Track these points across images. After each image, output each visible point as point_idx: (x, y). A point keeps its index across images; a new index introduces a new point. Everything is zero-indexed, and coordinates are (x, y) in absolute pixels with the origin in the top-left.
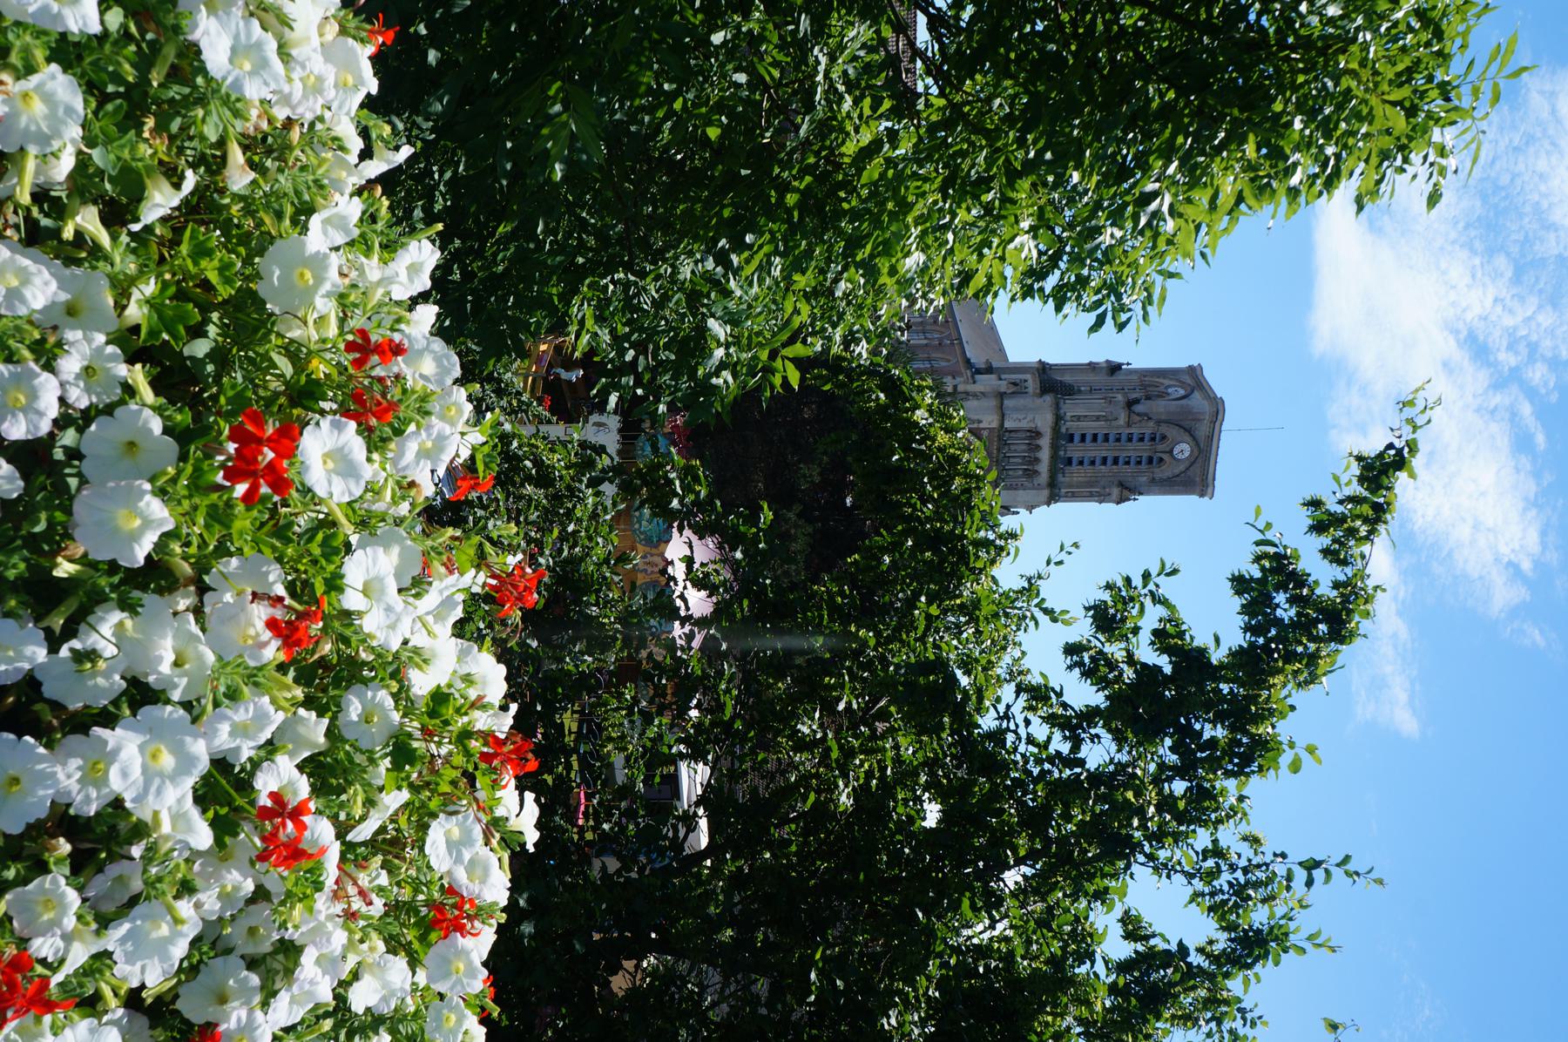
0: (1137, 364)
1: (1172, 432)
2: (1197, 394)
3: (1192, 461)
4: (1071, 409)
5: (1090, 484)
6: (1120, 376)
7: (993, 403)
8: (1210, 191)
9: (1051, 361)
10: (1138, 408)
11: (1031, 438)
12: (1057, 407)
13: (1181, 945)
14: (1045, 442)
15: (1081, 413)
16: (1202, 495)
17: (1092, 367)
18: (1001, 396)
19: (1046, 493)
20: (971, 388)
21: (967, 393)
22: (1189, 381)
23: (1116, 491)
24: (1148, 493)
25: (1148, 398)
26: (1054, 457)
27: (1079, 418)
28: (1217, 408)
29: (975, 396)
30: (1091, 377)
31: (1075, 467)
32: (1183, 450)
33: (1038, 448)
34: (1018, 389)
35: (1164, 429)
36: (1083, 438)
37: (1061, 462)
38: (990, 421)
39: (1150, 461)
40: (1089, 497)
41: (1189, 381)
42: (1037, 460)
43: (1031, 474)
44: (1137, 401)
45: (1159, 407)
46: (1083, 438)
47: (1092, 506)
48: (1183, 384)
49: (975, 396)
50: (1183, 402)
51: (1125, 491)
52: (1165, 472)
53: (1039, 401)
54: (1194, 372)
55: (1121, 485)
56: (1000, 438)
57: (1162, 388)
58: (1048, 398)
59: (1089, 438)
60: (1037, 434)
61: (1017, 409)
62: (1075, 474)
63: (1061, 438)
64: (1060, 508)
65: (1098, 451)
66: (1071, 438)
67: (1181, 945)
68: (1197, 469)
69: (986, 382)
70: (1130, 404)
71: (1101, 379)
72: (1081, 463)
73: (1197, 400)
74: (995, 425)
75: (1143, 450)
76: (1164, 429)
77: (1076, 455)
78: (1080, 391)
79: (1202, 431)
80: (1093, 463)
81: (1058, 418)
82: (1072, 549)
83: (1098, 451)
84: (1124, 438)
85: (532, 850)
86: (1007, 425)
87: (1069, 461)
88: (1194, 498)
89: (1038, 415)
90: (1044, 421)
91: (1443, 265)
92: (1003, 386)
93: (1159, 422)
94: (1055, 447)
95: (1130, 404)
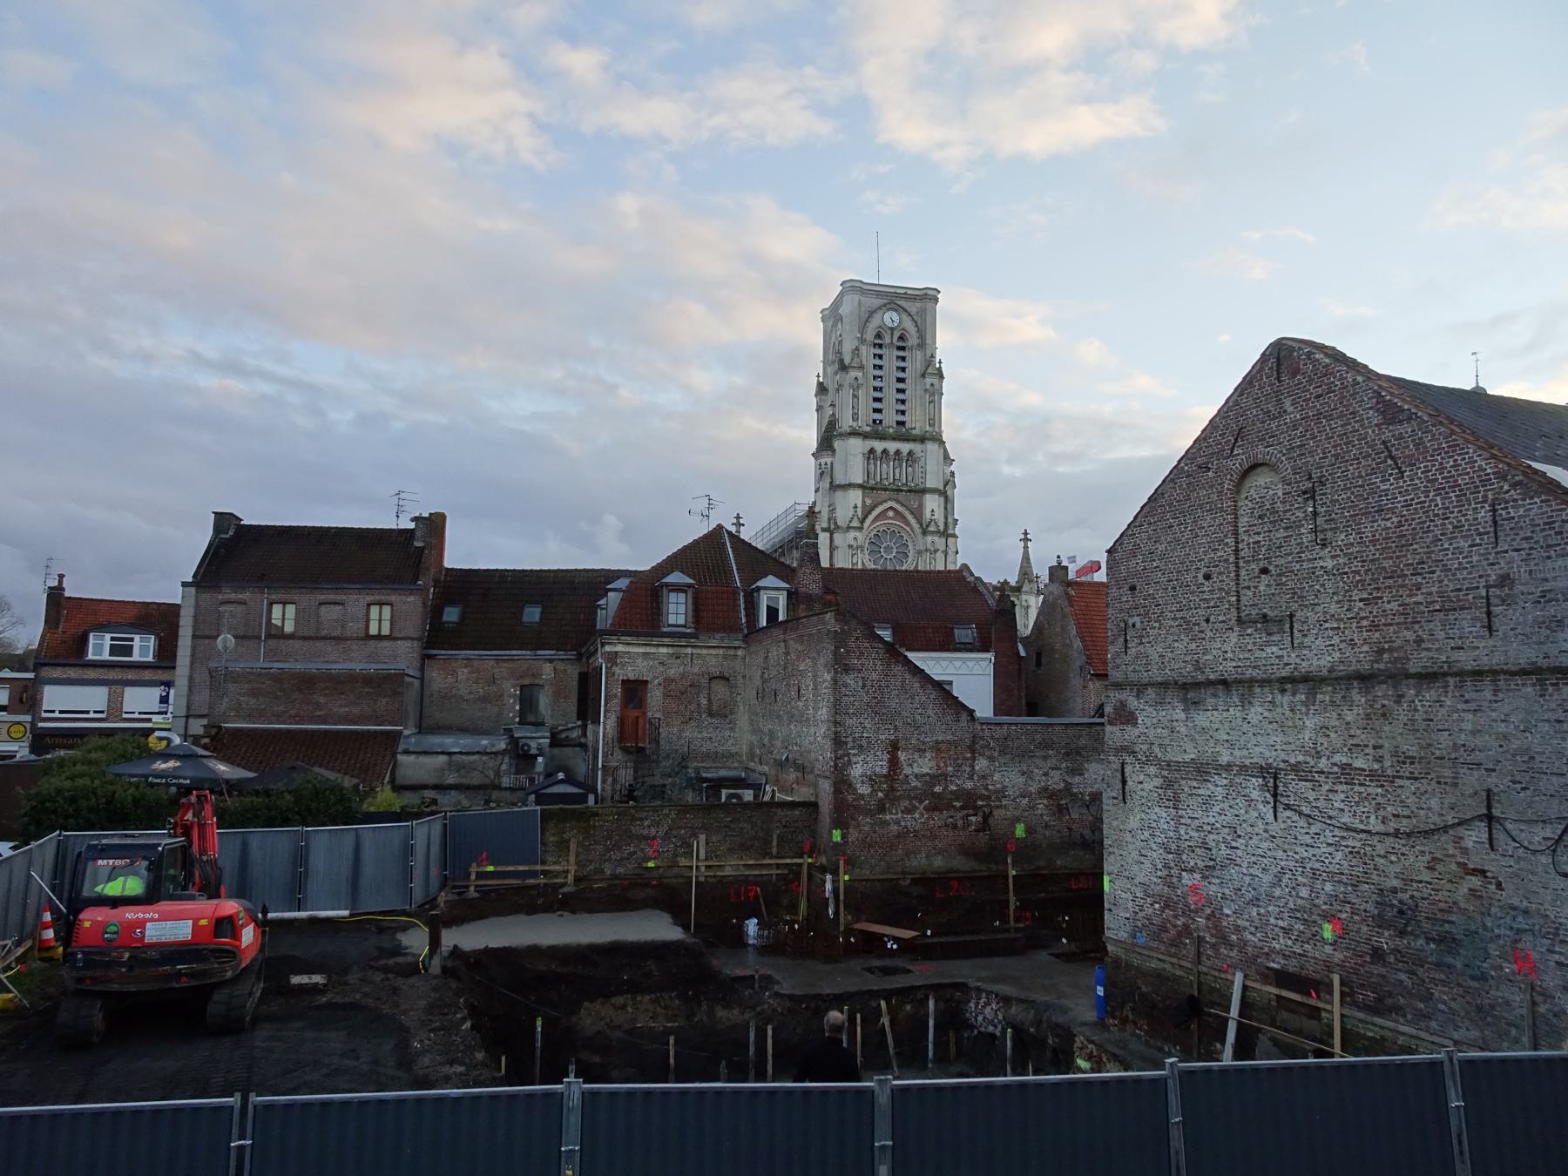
4: (846, 423)
7: (839, 494)
10: (847, 360)
14: (879, 446)
35: (870, 336)
58: (837, 444)
65: (890, 395)
74: (859, 493)
75: (890, 355)
81: (854, 433)
83: (890, 395)
90: (857, 446)
93: (862, 341)
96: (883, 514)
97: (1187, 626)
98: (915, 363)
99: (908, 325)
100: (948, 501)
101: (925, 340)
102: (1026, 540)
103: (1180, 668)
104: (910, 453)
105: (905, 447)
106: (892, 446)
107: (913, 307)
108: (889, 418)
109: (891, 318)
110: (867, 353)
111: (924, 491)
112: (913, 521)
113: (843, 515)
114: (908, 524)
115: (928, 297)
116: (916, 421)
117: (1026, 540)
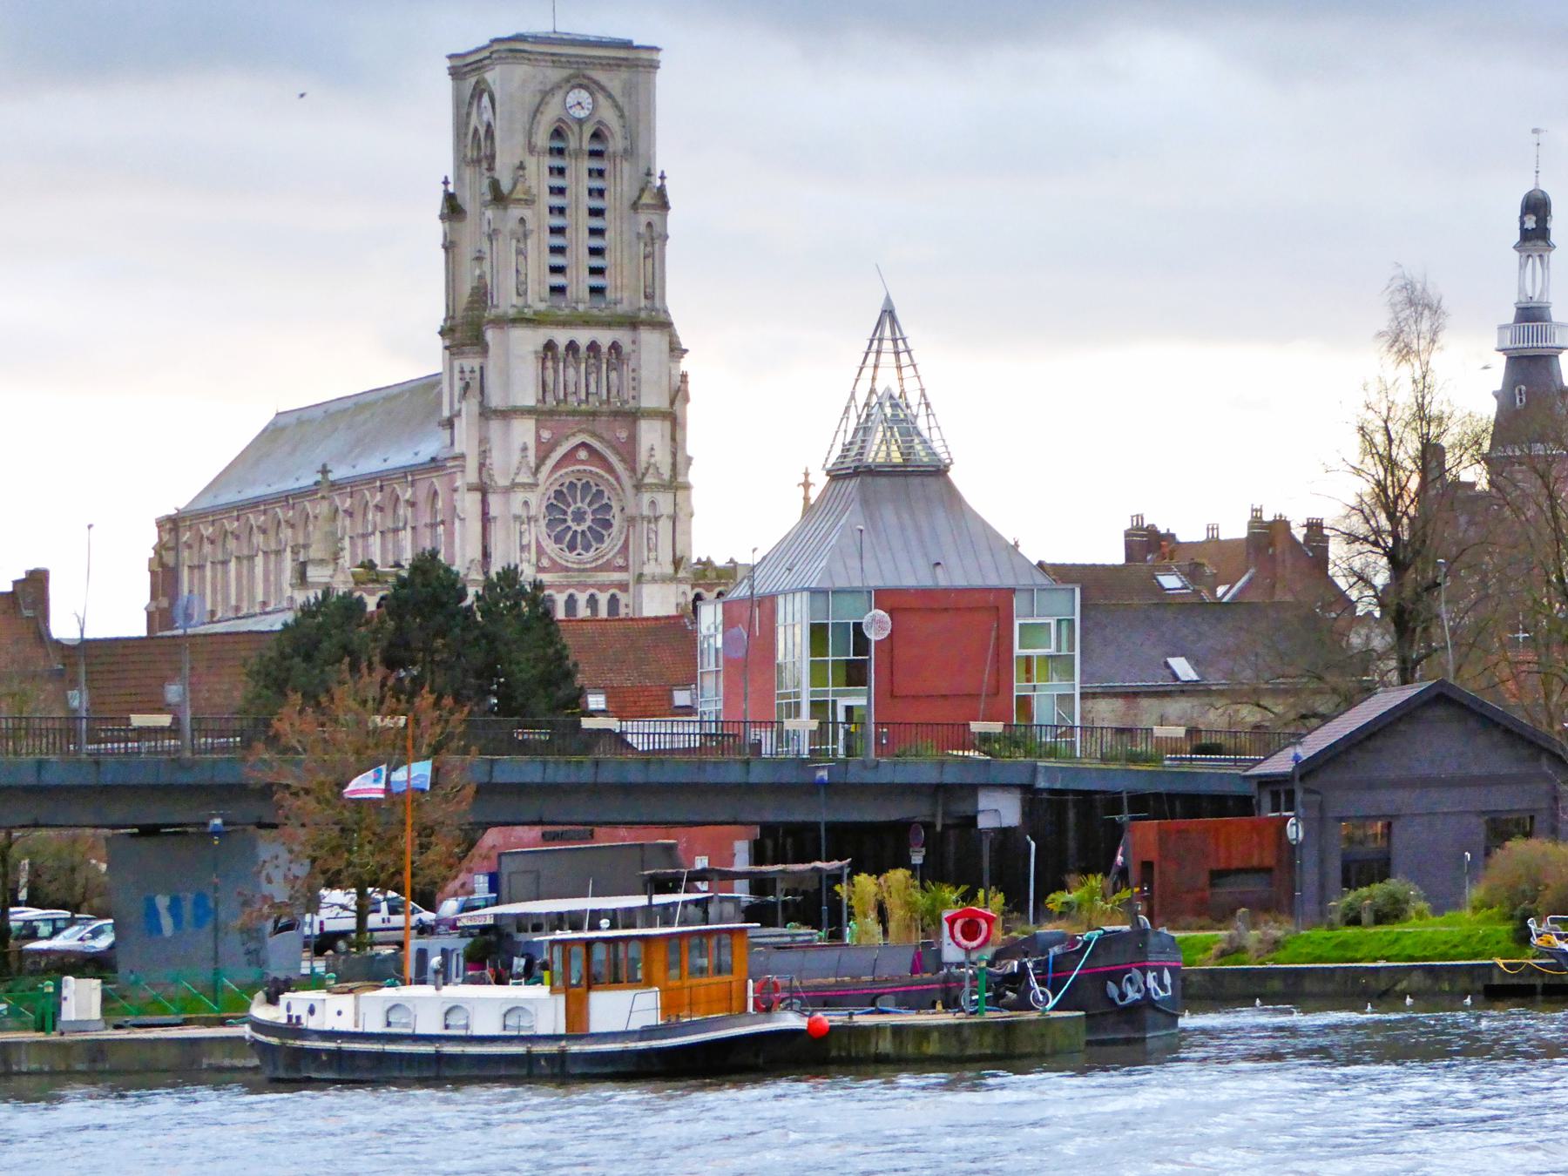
4: (506, 300)
6: (467, 201)
7: (495, 426)
8: (41, 924)
9: (441, 314)
10: (506, 186)
11: (555, 359)
13: (1315, 527)
14: (562, 337)
15: (520, 277)
16: (653, 66)
18: (486, 413)
20: (472, 464)
21: (482, 466)
24: (650, 158)
29: (484, 454)
38: (524, 431)
44: (495, 185)
49: (484, 454)
58: (490, 335)
59: (558, 261)
61: (506, 385)
66: (558, 290)
67: (1315, 527)
78: (481, 277)
80: (596, 252)
84: (557, 201)
85: (1474, 475)
86: (530, 401)
87: (596, 291)
90: (527, 341)
92: (470, 407)
95: (499, 198)
96: (569, 457)
98: (621, 187)
99: (608, 115)
101: (637, 148)
104: (615, 347)
105: (605, 337)
106: (583, 337)
107: (613, 81)
109: (579, 102)
114: (610, 469)
115: (634, 61)
116: (623, 293)
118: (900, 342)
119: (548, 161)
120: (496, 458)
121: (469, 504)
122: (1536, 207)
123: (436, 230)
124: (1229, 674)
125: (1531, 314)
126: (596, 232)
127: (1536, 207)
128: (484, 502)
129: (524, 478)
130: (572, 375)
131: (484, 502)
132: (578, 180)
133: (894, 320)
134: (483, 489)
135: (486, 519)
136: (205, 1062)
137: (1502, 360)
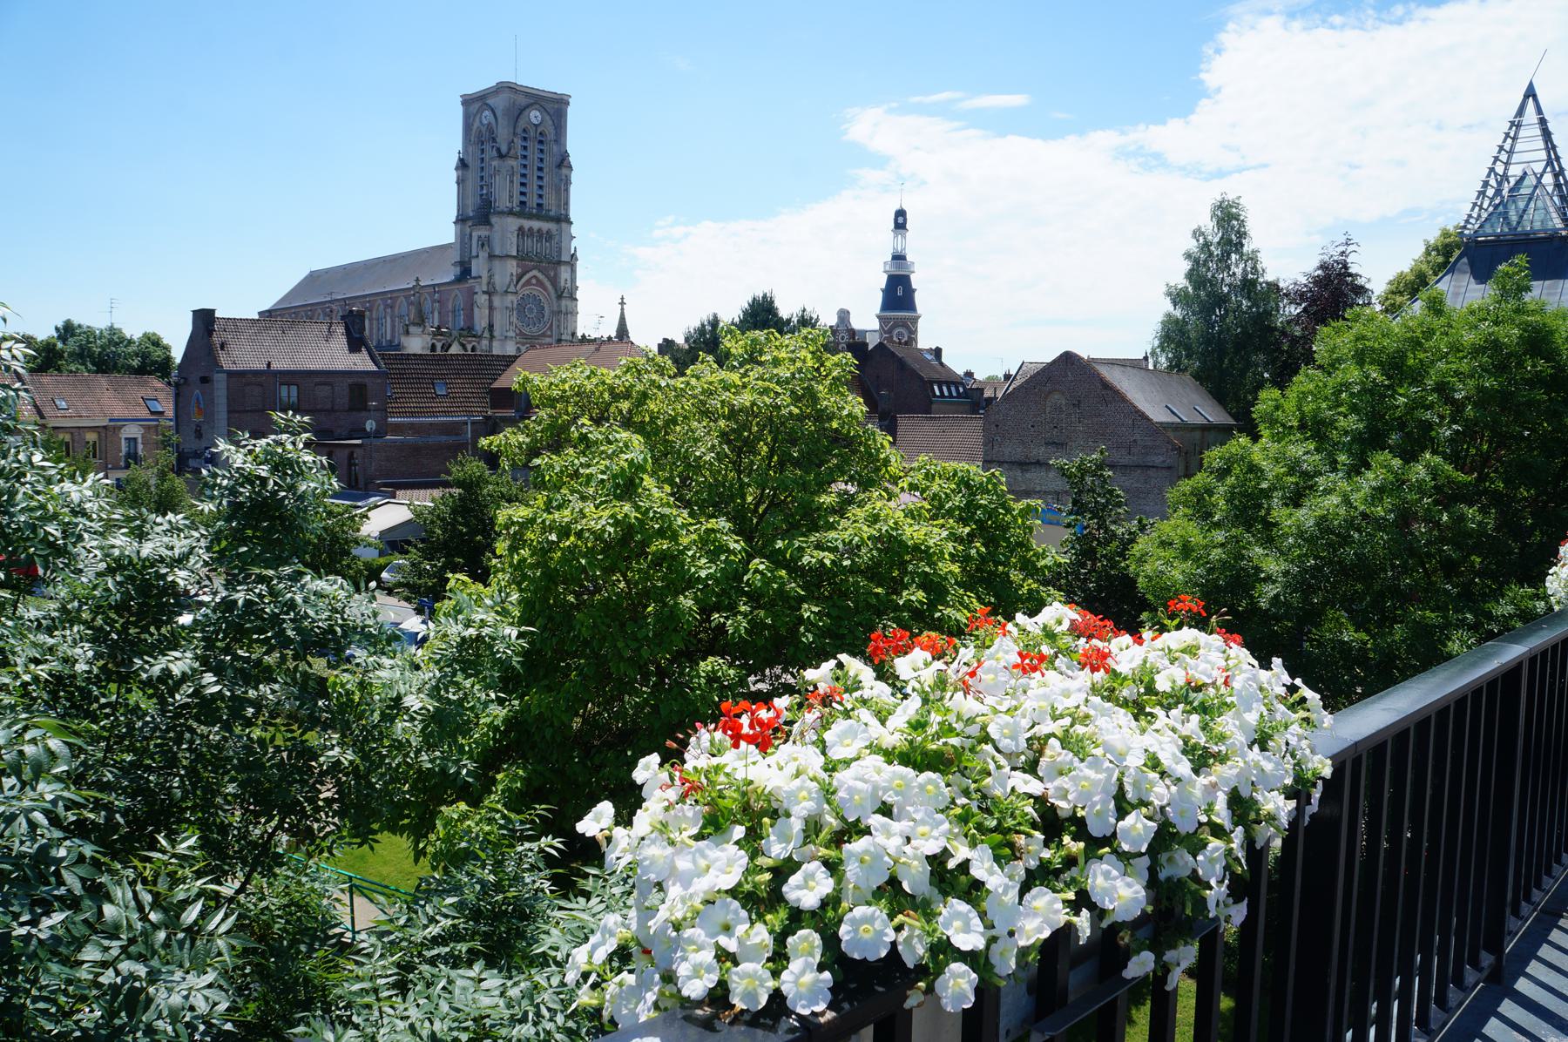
0: (458, 144)
1: (522, 124)
2: (490, 101)
3: (543, 109)
4: (503, 200)
5: (558, 191)
6: (469, 161)
7: (497, 263)
10: (504, 149)
12: (502, 213)
14: (527, 224)
16: (568, 103)
17: (460, 182)
18: (491, 257)
19: (564, 225)
20: (485, 280)
22: (477, 106)
23: (564, 171)
25: (494, 140)
26: (538, 217)
27: (511, 197)
28: (504, 88)
30: (469, 183)
31: (544, 202)
32: (535, 116)
33: (531, 229)
34: (485, 243)
35: (519, 130)
36: (523, 194)
37: (540, 213)
38: (512, 267)
39: (541, 142)
40: (567, 190)
41: (477, 106)
42: (539, 230)
43: (549, 236)
44: (498, 150)
45: (503, 134)
46: (523, 194)
47: (573, 189)
48: (480, 111)
49: (490, 277)
50: (499, 114)
51: (563, 162)
52: (549, 129)
53: (496, 227)
54: (467, 101)
55: (560, 166)
56: (523, 259)
57: (484, 129)
58: (494, 219)
60: (521, 229)
62: (550, 201)
63: (522, 211)
64: (573, 214)
65: (533, 183)
66: (523, 203)
68: (548, 106)
69: (479, 267)
70: (501, 156)
71: (472, 175)
72: (540, 196)
73: (498, 102)
74: (514, 263)
75: (533, 147)
76: (519, 130)
77: (536, 200)
79: (523, 101)
80: (541, 187)
81: (511, 213)
82: (774, 766)
83: (533, 183)
87: (539, 205)
88: (569, 109)
89: (506, 231)
90: (513, 223)
91: (1083, 921)
92: (483, 255)
93: (515, 134)
94: (530, 217)
96: (528, 283)
97: (1023, 443)
98: (549, 162)
100: (573, 271)
102: (622, 303)
103: (1019, 457)
106: (536, 225)
108: (532, 201)
110: (519, 142)
111: (560, 263)
112: (548, 284)
113: (501, 280)
114: (545, 289)
117: (622, 303)
118: (1509, 141)
119: (538, 146)
120: (497, 279)
121: (482, 299)
122: (901, 213)
123: (453, 176)
124: (1435, 571)
125: (899, 258)
126: (540, 178)
127: (901, 213)
128: (490, 301)
129: (512, 289)
130: (528, 243)
131: (490, 301)
132: (533, 154)
133: (1535, 97)
134: (490, 293)
135: (491, 308)
136: (362, 362)
137: (885, 277)
